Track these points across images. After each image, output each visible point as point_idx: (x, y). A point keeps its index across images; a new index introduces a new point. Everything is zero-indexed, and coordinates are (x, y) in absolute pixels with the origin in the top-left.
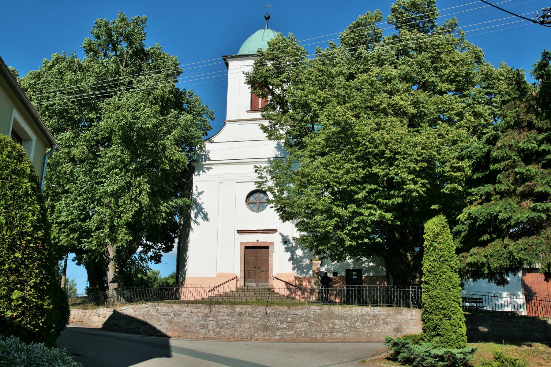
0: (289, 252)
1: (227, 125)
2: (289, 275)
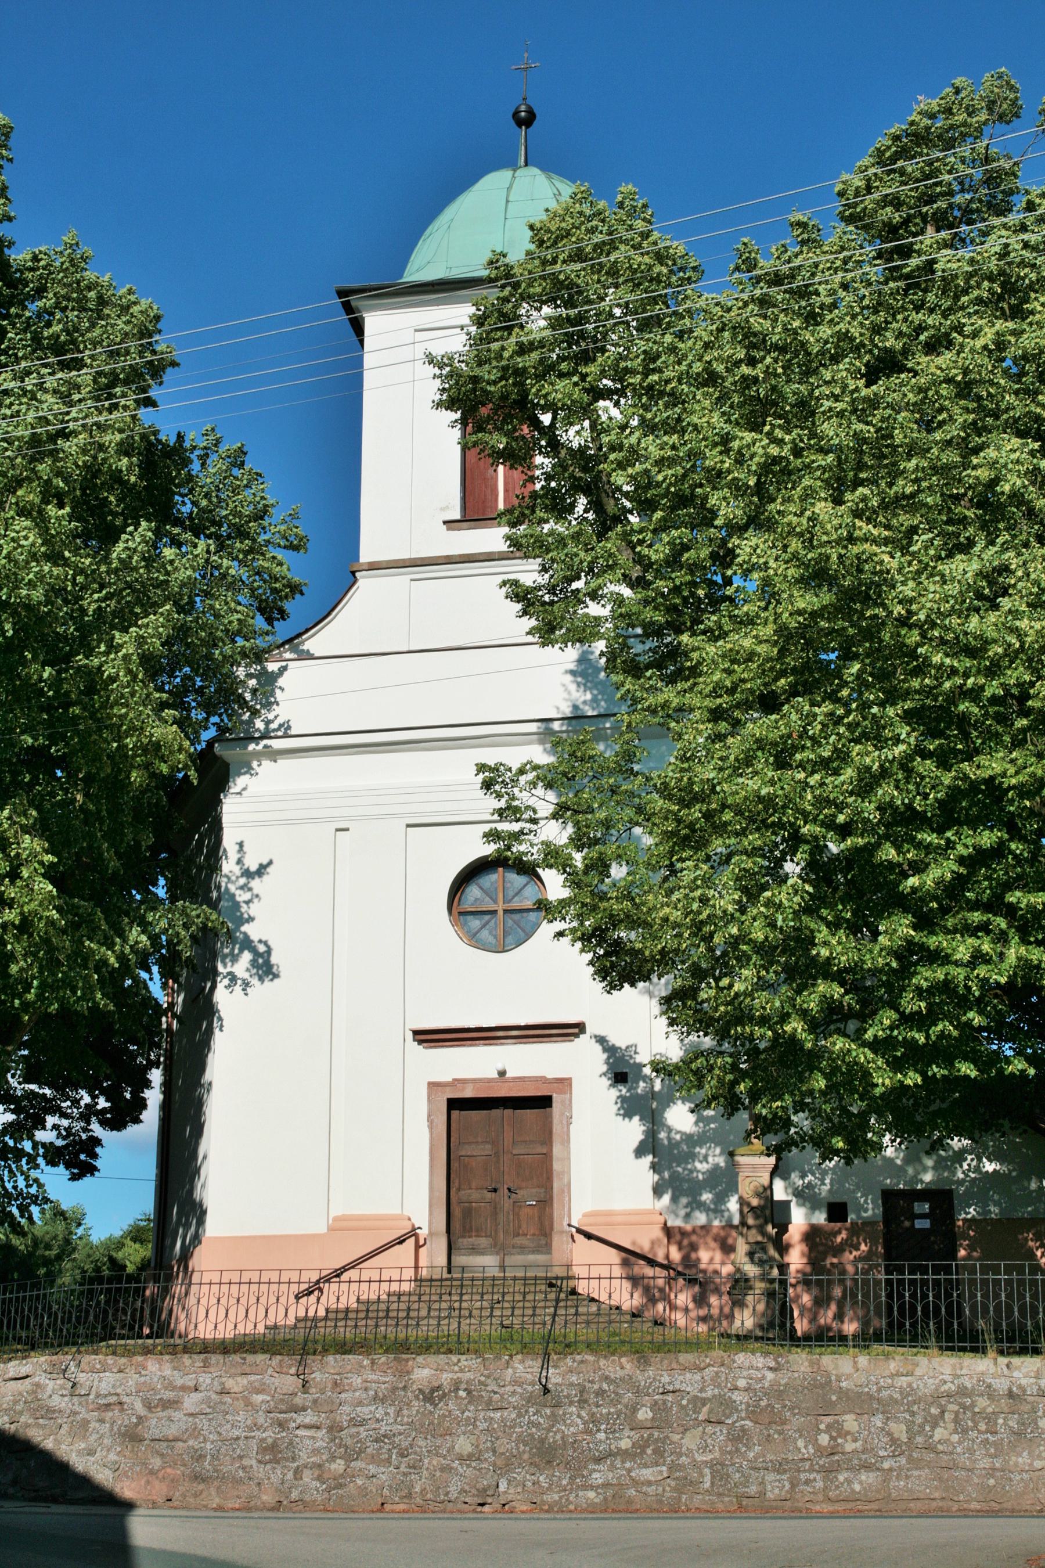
0: (636, 1119)
1: (365, 583)
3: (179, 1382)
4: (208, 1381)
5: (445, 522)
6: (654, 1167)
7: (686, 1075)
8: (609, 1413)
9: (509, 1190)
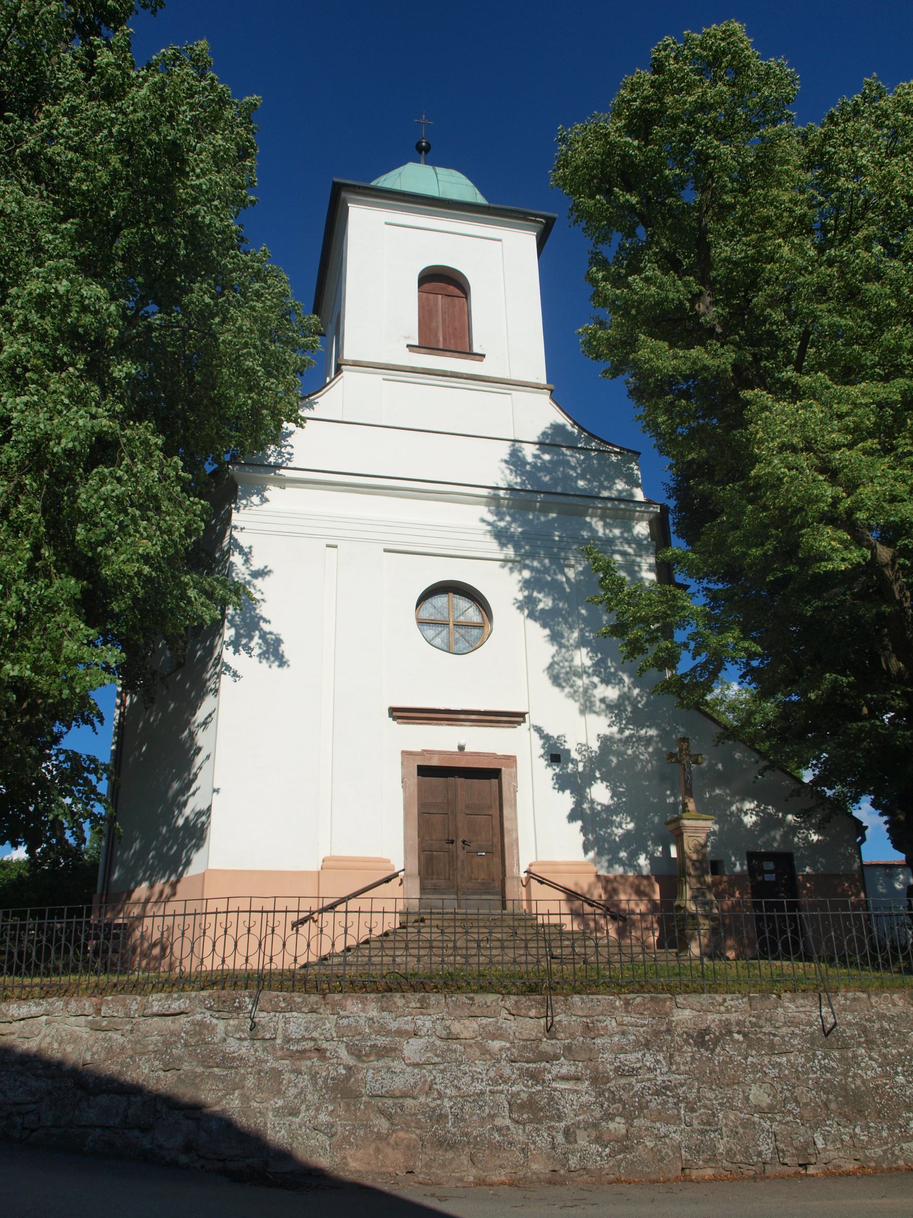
0: (568, 792)
1: (348, 374)
2: (573, 868)
3: (393, 1026)
4: (429, 1024)
5: (408, 346)
6: (584, 830)
7: (604, 761)
8: (900, 1054)
9: (464, 842)
